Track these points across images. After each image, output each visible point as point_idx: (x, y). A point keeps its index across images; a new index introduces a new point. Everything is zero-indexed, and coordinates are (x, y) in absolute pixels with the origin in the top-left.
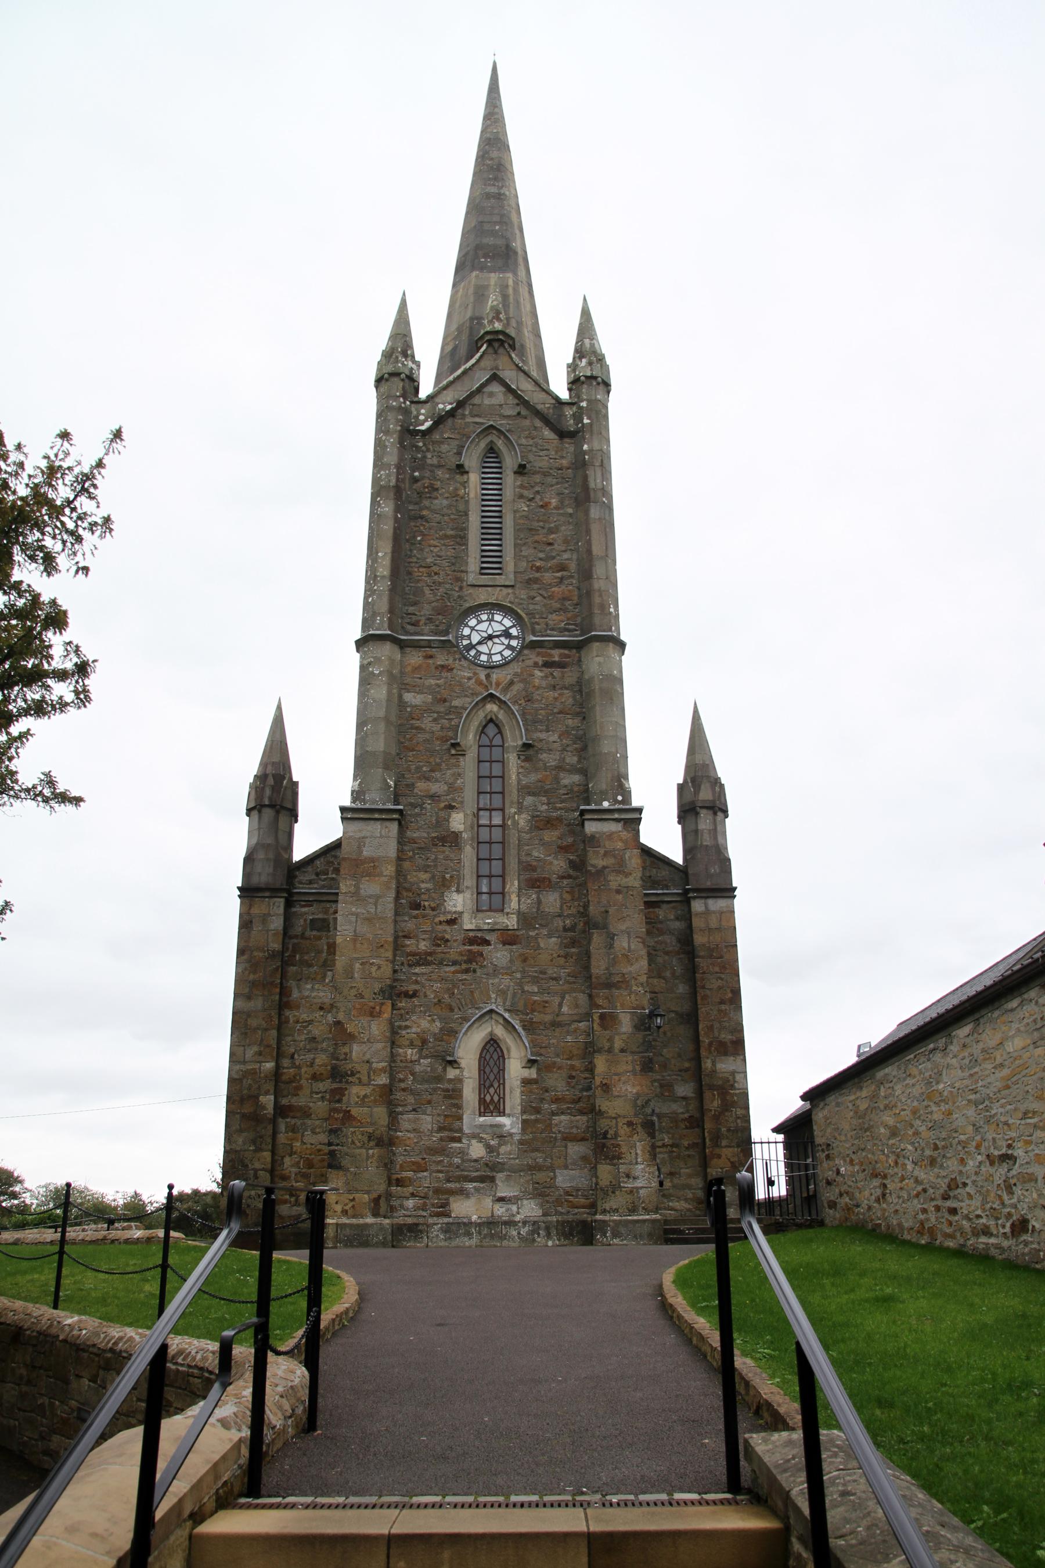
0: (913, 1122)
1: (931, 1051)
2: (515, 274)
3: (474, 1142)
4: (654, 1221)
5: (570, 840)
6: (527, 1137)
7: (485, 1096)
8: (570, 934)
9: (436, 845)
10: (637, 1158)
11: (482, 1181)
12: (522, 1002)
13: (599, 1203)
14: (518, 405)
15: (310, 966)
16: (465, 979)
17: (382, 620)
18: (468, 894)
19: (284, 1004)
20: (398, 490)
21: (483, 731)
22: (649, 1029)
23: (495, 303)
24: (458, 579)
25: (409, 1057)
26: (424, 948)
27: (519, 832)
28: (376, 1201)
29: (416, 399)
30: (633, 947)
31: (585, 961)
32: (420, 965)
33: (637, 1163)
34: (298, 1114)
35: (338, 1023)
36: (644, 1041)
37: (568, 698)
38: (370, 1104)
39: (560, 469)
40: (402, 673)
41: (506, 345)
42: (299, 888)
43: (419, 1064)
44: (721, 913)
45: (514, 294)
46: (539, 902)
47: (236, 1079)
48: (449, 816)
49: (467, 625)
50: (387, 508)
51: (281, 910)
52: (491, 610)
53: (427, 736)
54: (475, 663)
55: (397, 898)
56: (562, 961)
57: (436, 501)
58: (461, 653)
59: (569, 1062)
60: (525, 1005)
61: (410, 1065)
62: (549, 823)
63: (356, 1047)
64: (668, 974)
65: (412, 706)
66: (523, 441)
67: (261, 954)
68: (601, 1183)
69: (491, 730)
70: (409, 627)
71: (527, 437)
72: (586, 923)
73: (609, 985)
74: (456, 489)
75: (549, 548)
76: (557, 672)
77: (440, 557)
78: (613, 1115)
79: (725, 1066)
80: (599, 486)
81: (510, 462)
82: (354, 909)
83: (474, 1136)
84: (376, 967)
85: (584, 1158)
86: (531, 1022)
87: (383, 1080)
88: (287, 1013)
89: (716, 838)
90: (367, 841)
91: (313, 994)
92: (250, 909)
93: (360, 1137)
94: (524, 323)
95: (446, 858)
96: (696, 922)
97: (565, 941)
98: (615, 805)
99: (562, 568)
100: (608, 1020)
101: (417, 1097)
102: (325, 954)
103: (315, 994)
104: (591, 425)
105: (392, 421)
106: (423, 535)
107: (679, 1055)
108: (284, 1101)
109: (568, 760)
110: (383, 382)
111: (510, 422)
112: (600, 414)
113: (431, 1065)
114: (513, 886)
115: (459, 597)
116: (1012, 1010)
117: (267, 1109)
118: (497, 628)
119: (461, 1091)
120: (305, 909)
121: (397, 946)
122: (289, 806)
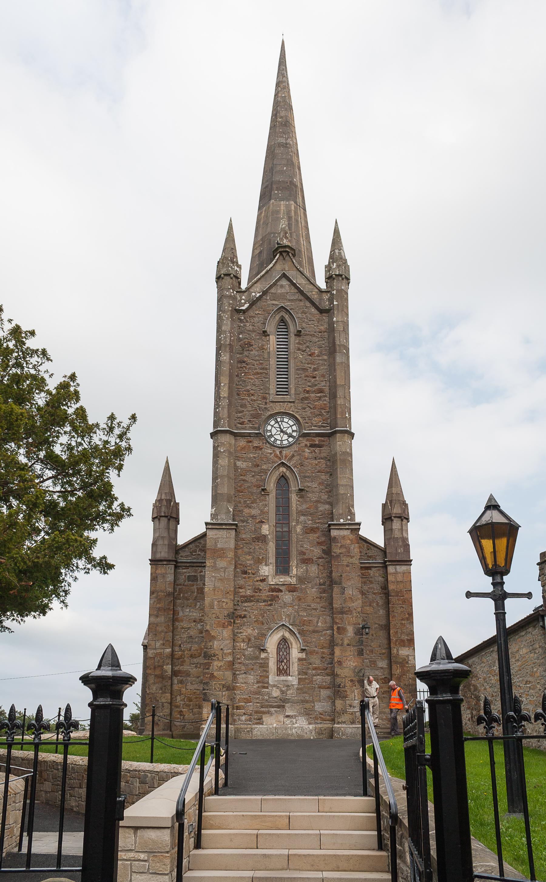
0: (484, 684)
1: (491, 652)
6: (301, 686)
7: (280, 666)
9: (255, 541)
10: (355, 697)
11: (278, 708)
12: (298, 620)
13: (336, 719)
15: (188, 600)
16: (270, 609)
19: (174, 620)
22: (362, 634)
24: (265, 398)
25: (242, 647)
26: (249, 594)
27: (297, 535)
29: (239, 290)
30: (354, 594)
32: (247, 602)
33: (355, 700)
34: (184, 675)
36: (360, 640)
38: (224, 670)
40: (235, 451)
41: (290, 254)
42: (181, 559)
43: (247, 651)
45: (295, 215)
46: (307, 571)
47: (151, 658)
51: (173, 571)
52: (282, 416)
53: (249, 485)
54: (273, 445)
55: (236, 567)
56: (318, 600)
57: (252, 352)
59: (322, 650)
60: (300, 622)
61: (242, 651)
62: (313, 530)
67: (163, 594)
68: (337, 709)
69: (283, 481)
72: (331, 581)
73: (342, 613)
74: (263, 345)
77: (255, 385)
78: (344, 676)
79: (404, 652)
82: (213, 574)
84: (225, 603)
85: (329, 697)
86: (303, 631)
87: (230, 658)
88: (177, 624)
91: (190, 614)
92: (156, 570)
93: (218, 686)
95: (260, 548)
96: (390, 578)
97: (320, 590)
98: (346, 521)
99: (321, 391)
100: (341, 630)
101: (246, 667)
102: (196, 594)
103: (191, 614)
104: (338, 305)
105: (226, 304)
107: (380, 646)
108: (176, 668)
110: (221, 279)
111: (292, 304)
112: (343, 296)
113: (253, 651)
116: (523, 636)
117: (168, 673)
119: (268, 663)
121: (236, 593)
122: (174, 516)
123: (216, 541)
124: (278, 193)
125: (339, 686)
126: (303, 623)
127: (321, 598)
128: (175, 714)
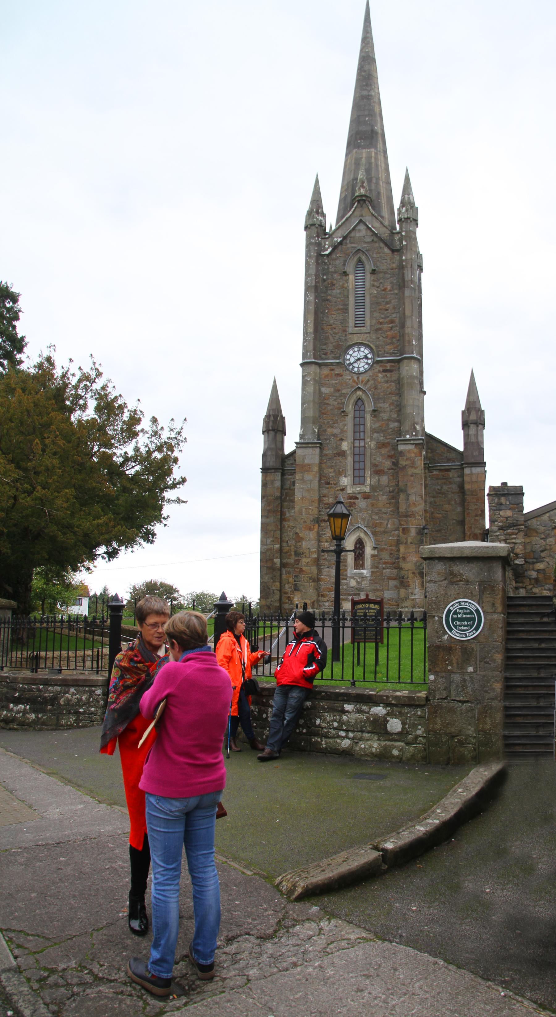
2: (376, 148)
3: (352, 580)
4: (422, 611)
5: (393, 453)
8: (392, 494)
14: (372, 235)
17: (310, 354)
18: (349, 478)
19: (282, 519)
20: (316, 287)
21: (356, 403)
23: (362, 177)
27: (371, 450)
28: (313, 603)
31: (397, 506)
35: (297, 533)
37: (393, 387)
39: (392, 269)
40: (320, 378)
44: (478, 474)
46: (379, 480)
48: (341, 443)
49: (348, 354)
50: (311, 298)
51: (279, 478)
53: (332, 407)
54: (352, 372)
56: (388, 505)
58: (346, 367)
63: (304, 543)
64: (453, 503)
65: (325, 394)
66: (375, 256)
67: (272, 498)
70: (323, 356)
71: (376, 253)
72: (398, 489)
73: (407, 516)
74: (343, 284)
75: (386, 312)
76: (388, 374)
80: (410, 279)
81: (369, 267)
83: (352, 578)
86: (375, 531)
87: (315, 556)
88: (284, 523)
89: (477, 438)
90: (307, 457)
94: (381, 178)
96: (466, 479)
99: (392, 322)
100: (406, 531)
104: (406, 245)
106: (329, 309)
108: (284, 561)
109: (393, 416)
114: (368, 473)
115: (345, 340)
118: (362, 354)
119: (346, 560)
120: (290, 477)
121: (320, 501)
122: (281, 429)
123: (304, 457)
124: (361, 142)
125: (403, 577)
126: (375, 525)
127: (390, 504)
128: (284, 600)
